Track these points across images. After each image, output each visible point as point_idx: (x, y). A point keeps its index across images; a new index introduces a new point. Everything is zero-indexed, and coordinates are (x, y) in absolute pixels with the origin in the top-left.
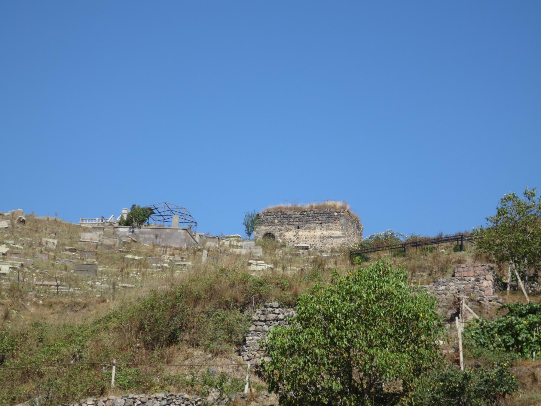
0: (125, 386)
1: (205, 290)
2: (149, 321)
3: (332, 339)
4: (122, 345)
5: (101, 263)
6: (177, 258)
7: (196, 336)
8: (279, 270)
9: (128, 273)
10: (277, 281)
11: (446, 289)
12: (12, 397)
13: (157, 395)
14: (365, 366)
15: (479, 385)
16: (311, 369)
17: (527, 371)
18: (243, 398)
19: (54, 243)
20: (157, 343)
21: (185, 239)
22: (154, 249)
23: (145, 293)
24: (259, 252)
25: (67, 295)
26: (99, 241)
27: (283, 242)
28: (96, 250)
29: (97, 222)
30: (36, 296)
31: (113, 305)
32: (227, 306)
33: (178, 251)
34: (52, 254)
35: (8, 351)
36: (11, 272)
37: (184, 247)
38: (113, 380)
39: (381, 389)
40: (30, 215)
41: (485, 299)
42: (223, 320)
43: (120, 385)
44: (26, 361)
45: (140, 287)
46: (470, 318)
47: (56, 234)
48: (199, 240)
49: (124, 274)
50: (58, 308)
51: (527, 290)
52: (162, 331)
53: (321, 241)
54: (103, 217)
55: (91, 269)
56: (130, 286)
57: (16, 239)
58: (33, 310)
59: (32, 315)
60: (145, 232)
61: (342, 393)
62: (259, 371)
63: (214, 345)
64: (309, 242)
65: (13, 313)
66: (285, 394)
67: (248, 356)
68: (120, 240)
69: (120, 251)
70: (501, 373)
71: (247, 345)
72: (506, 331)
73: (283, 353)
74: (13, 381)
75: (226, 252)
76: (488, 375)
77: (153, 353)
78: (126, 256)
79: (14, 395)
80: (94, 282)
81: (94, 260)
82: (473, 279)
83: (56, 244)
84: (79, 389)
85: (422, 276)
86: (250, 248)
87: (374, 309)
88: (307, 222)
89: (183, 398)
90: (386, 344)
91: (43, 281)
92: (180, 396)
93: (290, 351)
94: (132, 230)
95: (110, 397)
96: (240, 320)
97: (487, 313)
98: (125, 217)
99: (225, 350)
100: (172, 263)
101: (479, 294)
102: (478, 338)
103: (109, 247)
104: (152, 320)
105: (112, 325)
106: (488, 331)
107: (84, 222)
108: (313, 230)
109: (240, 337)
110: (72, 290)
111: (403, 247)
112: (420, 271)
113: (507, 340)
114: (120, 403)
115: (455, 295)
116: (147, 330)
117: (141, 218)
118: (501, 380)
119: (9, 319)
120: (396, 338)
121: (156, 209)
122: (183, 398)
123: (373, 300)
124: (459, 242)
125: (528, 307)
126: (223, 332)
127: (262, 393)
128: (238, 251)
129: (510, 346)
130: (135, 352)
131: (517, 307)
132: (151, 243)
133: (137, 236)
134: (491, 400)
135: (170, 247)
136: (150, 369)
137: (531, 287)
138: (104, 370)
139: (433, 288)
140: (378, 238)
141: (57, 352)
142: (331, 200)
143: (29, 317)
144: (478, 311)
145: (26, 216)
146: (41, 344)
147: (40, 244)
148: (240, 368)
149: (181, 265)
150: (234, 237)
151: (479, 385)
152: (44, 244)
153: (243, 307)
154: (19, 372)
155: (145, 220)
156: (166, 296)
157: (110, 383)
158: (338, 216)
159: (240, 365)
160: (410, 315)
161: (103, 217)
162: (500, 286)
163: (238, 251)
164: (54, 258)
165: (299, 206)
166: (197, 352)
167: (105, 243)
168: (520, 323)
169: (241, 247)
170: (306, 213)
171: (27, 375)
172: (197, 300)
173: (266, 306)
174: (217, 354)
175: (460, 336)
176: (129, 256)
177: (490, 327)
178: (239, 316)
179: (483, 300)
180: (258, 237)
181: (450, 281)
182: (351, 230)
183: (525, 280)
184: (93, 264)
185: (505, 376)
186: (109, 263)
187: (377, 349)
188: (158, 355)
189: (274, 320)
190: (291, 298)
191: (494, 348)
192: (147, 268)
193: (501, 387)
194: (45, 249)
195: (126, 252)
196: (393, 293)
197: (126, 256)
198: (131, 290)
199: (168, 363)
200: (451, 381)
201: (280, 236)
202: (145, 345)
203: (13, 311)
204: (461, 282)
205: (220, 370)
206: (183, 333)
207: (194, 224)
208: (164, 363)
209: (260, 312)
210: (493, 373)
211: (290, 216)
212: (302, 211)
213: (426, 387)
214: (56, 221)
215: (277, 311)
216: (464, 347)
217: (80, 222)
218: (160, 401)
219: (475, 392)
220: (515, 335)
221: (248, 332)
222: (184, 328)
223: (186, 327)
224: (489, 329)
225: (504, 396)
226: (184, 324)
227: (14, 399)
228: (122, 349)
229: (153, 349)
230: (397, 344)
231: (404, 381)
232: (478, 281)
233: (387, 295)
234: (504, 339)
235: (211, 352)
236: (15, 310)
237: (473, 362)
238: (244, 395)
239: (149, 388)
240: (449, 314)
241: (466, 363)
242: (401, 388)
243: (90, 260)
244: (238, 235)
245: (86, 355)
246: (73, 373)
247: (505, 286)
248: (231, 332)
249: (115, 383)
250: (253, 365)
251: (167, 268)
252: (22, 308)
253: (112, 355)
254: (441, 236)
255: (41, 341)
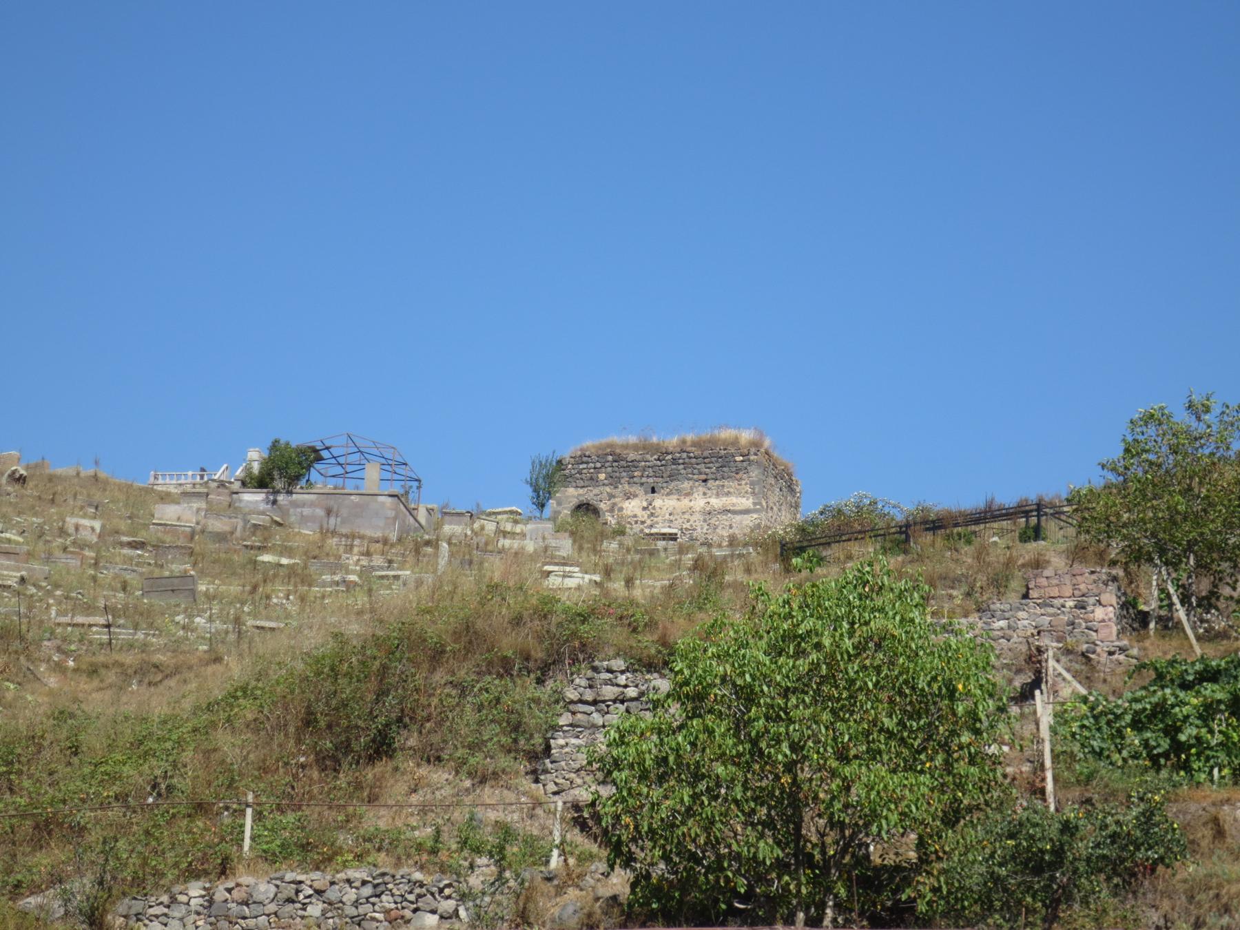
0: (274, 854)
1: (455, 633)
2: (327, 704)
4: (264, 761)
5: (202, 573)
6: (378, 561)
7: (436, 738)
9: (268, 597)
10: (619, 611)
11: (1009, 627)
12: (12, 880)
14: (830, 805)
15: (1098, 845)
17: (1200, 812)
18: (549, 879)
19: (93, 529)
20: (346, 754)
21: (395, 518)
22: (323, 540)
23: (314, 640)
24: (565, 546)
25: (131, 646)
26: (198, 523)
27: (618, 523)
28: (190, 544)
29: (190, 480)
30: (59, 649)
31: (236, 669)
32: (505, 668)
33: (379, 546)
34: (90, 554)
37: (393, 537)
38: (247, 842)
39: (867, 856)
40: (36, 466)
41: (1098, 650)
42: (498, 700)
43: (264, 851)
44: (42, 799)
45: (304, 626)
46: (1065, 692)
47: (97, 508)
48: (427, 521)
49: (257, 598)
50: (111, 677)
51: (1194, 628)
52: (357, 727)
53: (705, 521)
54: (203, 470)
55: (181, 587)
56: (273, 625)
58: (53, 681)
59: (51, 693)
60: (303, 503)
61: (781, 866)
62: (583, 818)
63: (476, 760)
64: (677, 523)
65: (8, 689)
66: (647, 871)
67: (556, 784)
68: (246, 521)
69: (246, 546)
70: (1147, 819)
71: (553, 758)
72: (1150, 722)
73: (644, 776)
74: (14, 843)
75: (490, 548)
76: (1118, 823)
77: (336, 778)
78: (260, 558)
79: (19, 877)
80: (191, 617)
81: (188, 566)
82: (1070, 603)
83: (98, 531)
84: (170, 861)
85: (951, 597)
86: (544, 538)
87: (852, 674)
88: (673, 477)
89: (409, 881)
90: (880, 752)
91: (73, 617)
92: (402, 877)
93: (662, 771)
94: (271, 498)
95: (241, 880)
96: (537, 701)
97: (1105, 681)
98: (256, 468)
99: (503, 771)
100: (365, 572)
101: (1084, 639)
102: (1087, 738)
103: (221, 537)
104: (334, 702)
106: (1109, 723)
107: (160, 481)
108: (688, 494)
109: (538, 740)
111: (901, 533)
112: (946, 587)
113: (1153, 743)
114: (266, 892)
115: (1031, 640)
117: (293, 471)
118: (1147, 833)
120: (902, 739)
121: (327, 448)
122: (409, 881)
123: (848, 652)
124: (1031, 519)
125: (1198, 667)
126: (498, 730)
127: (593, 868)
128: (516, 544)
129: (1159, 755)
130: (295, 776)
131: (1173, 667)
132: (316, 527)
133: (284, 512)
134: (1124, 880)
135: (362, 537)
136: (329, 815)
137: (1202, 621)
138: (226, 818)
139: (980, 624)
140: (840, 511)
141: (114, 778)
142: (728, 427)
143: (46, 699)
144: (1083, 676)
145: (27, 468)
146: (75, 760)
147: (62, 532)
149: (386, 577)
150: (505, 512)
151: (1098, 845)
152: (71, 530)
154: (29, 823)
155: (303, 475)
156: (363, 647)
157: (241, 847)
158: (745, 464)
159: (537, 803)
160: (935, 686)
161: (203, 470)
162: (1135, 619)
163: (516, 544)
164: (96, 564)
165: (655, 440)
166: (440, 776)
167: (210, 529)
168: (1183, 703)
169: (523, 535)
170: (669, 457)
172: (437, 656)
174: (483, 781)
175: (1045, 733)
176: (266, 558)
177: (1114, 714)
178: (532, 691)
179: (1094, 652)
180: (560, 512)
181: (1019, 609)
182: (775, 496)
183: (1190, 604)
184: (184, 576)
185: (1157, 825)
186: (221, 573)
187: (860, 765)
188: (349, 784)
189: (615, 701)
190: (653, 651)
191: (1124, 760)
192: (310, 585)
193: (1147, 850)
194: (74, 543)
195: (259, 548)
196: (893, 636)
197: (260, 558)
198: (269, 635)
199: (372, 800)
200: (1032, 837)
201: (611, 510)
202: (317, 761)
203: (7, 684)
204: (1042, 611)
205: (492, 815)
207: (415, 484)
208: (363, 800)
209: (584, 683)
210: (1129, 818)
211: (633, 465)
212: (662, 453)
213: (972, 854)
214: (95, 477)
215: (622, 679)
216: (1055, 757)
217: (152, 480)
218: (357, 888)
219: (1088, 860)
220: (1172, 731)
221: (555, 728)
222: (407, 720)
223: (411, 719)
224: (1111, 717)
225: (1153, 870)
226: (406, 712)
227: (18, 885)
228: (266, 770)
229: (335, 770)
230: (906, 752)
231: (921, 838)
232: (1084, 608)
234: (1147, 741)
235: (470, 775)
236: (12, 682)
237: (1076, 793)
238: (550, 872)
239: (330, 859)
240: (1017, 684)
241: (1060, 795)
242: (913, 855)
243: (177, 568)
244: (514, 508)
246: (153, 826)
247: (1144, 618)
248: (516, 729)
249: (251, 847)
250: (569, 805)
251: (356, 584)
253: (243, 783)
254: (989, 505)
255: (76, 754)
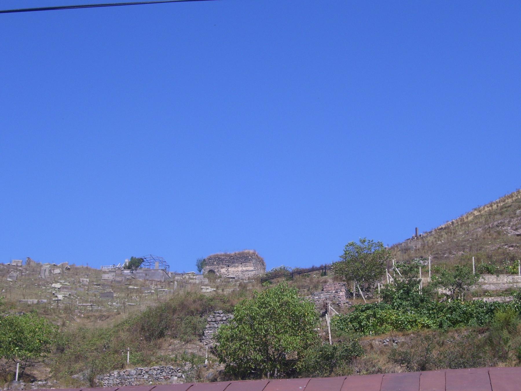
3: (255, 330)
6: (159, 287)
7: (175, 332)
8: (220, 291)
9: (132, 297)
13: (155, 367)
15: (342, 352)
16: (244, 348)
23: (143, 308)
24: (206, 281)
28: (112, 284)
30: (79, 312)
31: (124, 316)
32: (192, 313)
35: (66, 344)
36: (64, 299)
37: (163, 281)
38: (128, 360)
39: (285, 358)
42: (190, 322)
45: (144, 304)
46: (333, 314)
50: (93, 319)
55: (109, 295)
57: (65, 279)
58: (78, 320)
61: (263, 361)
63: (186, 337)
68: (125, 278)
70: (354, 345)
76: (347, 346)
82: (334, 292)
88: (233, 263)
93: (232, 338)
96: (201, 322)
100: (156, 290)
103: (119, 282)
105: (127, 326)
109: (201, 331)
110: (99, 308)
116: (146, 329)
119: (65, 326)
124: (323, 270)
130: (140, 343)
133: (135, 275)
147: (79, 282)
148: (202, 350)
151: (342, 352)
153: (202, 314)
154: (74, 357)
159: (201, 347)
162: (349, 295)
166: (176, 341)
169: (196, 279)
171: (78, 358)
172: (174, 311)
173: (215, 313)
174: (187, 342)
175: (329, 325)
176: (131, 287)
184: (110, 292)
201: (218, 272)
205: (190, 351)
206: (167, 331)
209: (212, 317)
215: (222, 315)
216: (331, 330)
220: (360, 323)
228: (132, 341)
233: (287, 303)
242: (296, 357)
245: (112, 345)
248: (195, 329)
252: (72, 320)
